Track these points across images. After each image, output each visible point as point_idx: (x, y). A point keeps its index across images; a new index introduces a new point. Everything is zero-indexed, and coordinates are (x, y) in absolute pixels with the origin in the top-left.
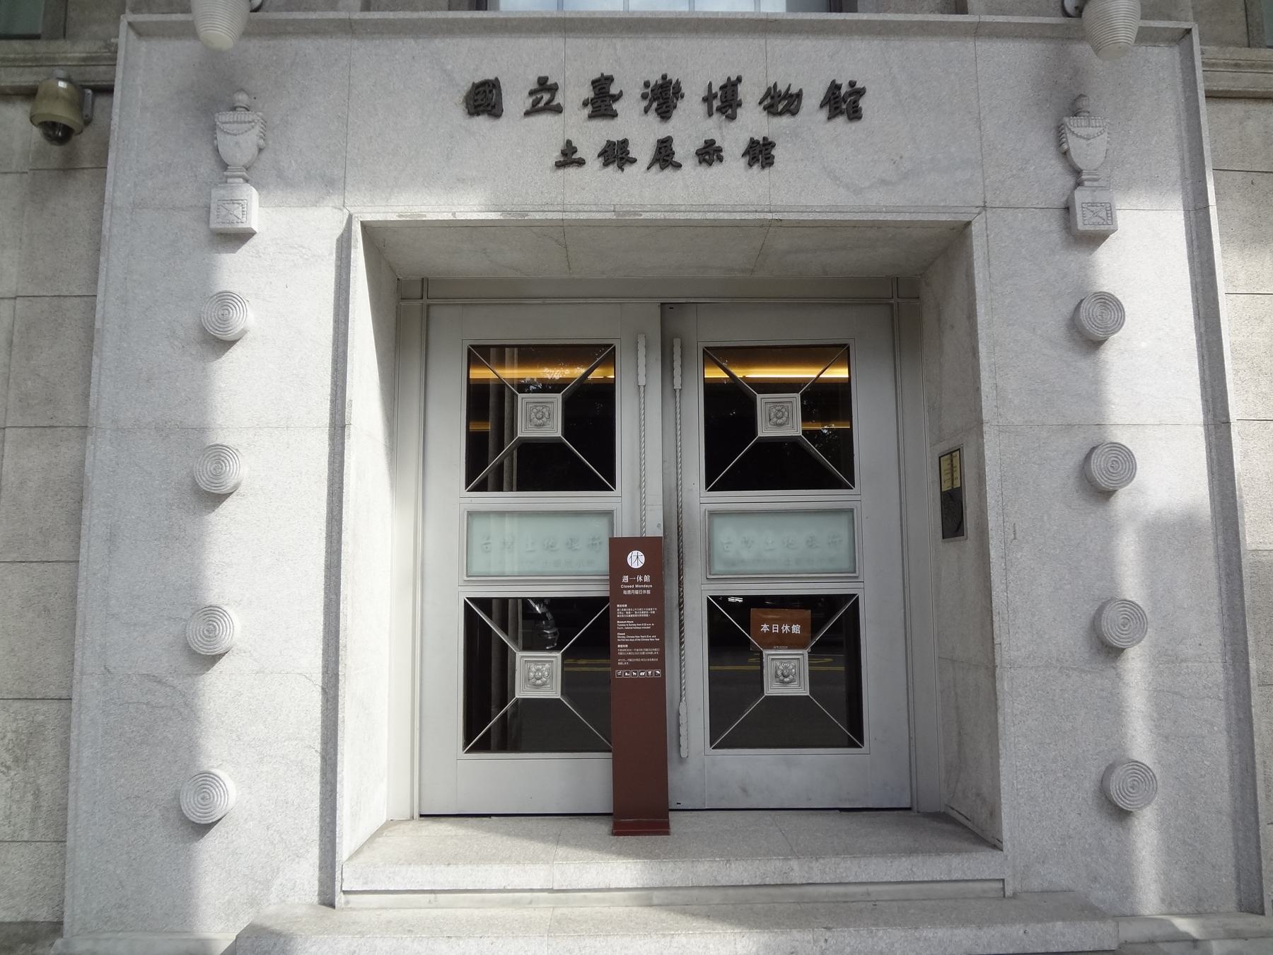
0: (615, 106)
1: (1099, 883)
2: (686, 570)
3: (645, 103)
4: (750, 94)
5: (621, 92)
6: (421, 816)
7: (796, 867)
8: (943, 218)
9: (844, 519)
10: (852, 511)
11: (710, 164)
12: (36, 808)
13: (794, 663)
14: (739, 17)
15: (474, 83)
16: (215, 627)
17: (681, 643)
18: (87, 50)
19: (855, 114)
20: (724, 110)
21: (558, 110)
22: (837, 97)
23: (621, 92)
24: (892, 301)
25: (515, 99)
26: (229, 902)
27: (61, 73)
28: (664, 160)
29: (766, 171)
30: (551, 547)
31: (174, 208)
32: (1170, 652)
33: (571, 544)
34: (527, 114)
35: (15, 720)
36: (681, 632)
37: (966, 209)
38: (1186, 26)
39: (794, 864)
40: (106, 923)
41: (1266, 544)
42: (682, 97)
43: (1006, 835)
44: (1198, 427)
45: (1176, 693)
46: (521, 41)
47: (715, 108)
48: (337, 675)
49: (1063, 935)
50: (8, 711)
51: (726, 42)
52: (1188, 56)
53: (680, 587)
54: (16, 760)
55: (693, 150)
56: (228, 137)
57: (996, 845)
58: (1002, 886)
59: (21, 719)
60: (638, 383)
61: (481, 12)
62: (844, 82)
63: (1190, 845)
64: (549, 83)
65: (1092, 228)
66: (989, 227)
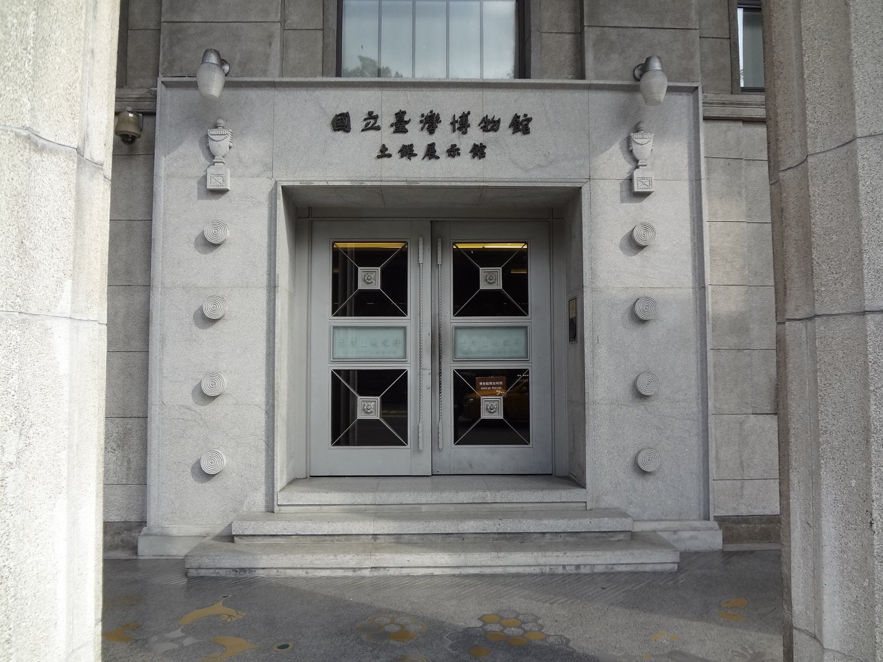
0: (407, 127)
1: (633, 505)
2: (443, 356)
3: (421, 125)
4: (474, 121)
5: (410, 119)
6: (311, 476)
7: (489, 495)
8: (568, 185)
9: (523, 332)
10: (526, 327)
11: (454, 157)
12: (129, 469)
13: (496, 403)
14: (469, 81)
15: (336, 115)
16: (215, 382)
17: (440, 393)
18: (140, 94)
19: (526, 131)
20: (461, 129)
21: (378, 128)
22: (517, 123)
23: (410, 119)
24: (549, 220)
25: (357, 123)
26: (224, 511)
27: (130, 109)
28: (431, 155)
29: (482, 160)
30: (374, 345)
31: (188, 177)
32: (671, 398)
33: (385, 343)
34: (363, 130)
35: (117, 427)
36: (440, 387)
37: (580, 180)
38: (695, 85)
39: (488, 493)
40: (166, 521)
41: (724, 346)
42: (440, 122)
43: (588, 481)
44: (691, 289)
45: (673, 417)
46: (360, 92)
47: (456, 128)
48: (273, 406)
49: (608, 524)
50: (113, 423)
51: (463, 93)
52: (696, 101)
53: (439, 365)
54: (118, 446)
55: (446, 149)
56: (214, 142)
57: (583, 486)
58: (585, 505)
59: (120, 427)
60: (419, 261)
61: (340, 78)
62: (521, 114)
63: (677, 488)
64: (373, 115)
65: (641, 190)
66: (591, 189)
